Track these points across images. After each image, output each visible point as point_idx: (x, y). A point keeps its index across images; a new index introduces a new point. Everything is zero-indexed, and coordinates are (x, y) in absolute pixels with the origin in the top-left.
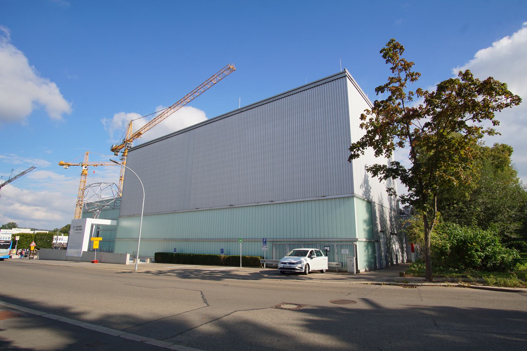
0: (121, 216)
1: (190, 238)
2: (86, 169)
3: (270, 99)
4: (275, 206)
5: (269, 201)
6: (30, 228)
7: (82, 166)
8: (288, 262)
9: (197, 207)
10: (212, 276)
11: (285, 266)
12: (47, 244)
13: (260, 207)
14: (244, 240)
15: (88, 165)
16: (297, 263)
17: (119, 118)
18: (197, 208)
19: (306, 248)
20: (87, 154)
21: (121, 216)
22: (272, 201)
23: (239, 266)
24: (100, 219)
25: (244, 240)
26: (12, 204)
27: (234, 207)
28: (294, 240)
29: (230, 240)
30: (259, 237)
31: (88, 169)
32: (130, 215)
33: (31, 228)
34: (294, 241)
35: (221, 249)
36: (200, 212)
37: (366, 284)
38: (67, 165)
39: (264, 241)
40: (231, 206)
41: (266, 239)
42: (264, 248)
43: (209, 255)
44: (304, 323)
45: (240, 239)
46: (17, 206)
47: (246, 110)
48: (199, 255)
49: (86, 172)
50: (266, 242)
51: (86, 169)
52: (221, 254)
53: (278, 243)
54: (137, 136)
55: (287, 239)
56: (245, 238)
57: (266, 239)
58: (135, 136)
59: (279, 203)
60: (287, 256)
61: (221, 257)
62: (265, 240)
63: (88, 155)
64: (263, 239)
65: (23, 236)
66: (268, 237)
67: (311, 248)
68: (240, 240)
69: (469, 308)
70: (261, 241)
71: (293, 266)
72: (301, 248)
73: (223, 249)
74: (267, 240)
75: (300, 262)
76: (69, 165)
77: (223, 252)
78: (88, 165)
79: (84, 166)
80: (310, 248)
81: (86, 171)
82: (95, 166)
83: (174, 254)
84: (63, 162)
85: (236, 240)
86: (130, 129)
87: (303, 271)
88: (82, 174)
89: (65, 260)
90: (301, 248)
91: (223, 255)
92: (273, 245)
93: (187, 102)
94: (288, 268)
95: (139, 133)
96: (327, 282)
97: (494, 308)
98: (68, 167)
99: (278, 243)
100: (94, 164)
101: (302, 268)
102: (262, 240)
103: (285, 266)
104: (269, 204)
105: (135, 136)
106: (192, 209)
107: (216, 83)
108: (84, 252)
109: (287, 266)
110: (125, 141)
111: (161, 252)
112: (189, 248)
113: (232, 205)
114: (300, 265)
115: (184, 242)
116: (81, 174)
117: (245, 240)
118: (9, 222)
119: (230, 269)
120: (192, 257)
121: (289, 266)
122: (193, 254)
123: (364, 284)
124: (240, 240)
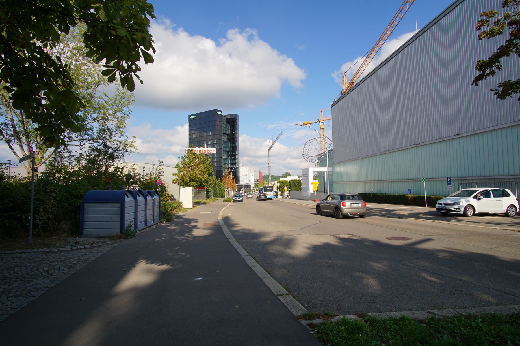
0: (334, 163)
1: (384, 179)
2: (323, 124)
3: (448, 8)
4: (461, 140)
5: (455, 135)
6: (297, 176)
7: (319, 122)
8: (443, 203)
9: (416, 142)
10: (390, 214)
11: (440, 207)
12: (298, 188)
13: (444, 143)
14: (428, 180)
15: (323, 121)
16: (454, 204)
17: (346, 67)
18: (387, 151)
19: (472, 188)
20: (321, 111)
21: (334, 163)
22: (458, 135)
23: (425, 206)
24: (320, 167)
25: (428, 180)
26: (286, 159)
27: (419, 146)
28: (515, 177)
29: (418, 180)
30: (443, 176)
31: (324, 124)
32: (339, 162)
33: (298, 175)
34: (485, 179)
35: (409, 189)
36: (390, 154)
37: (512, 230)
38: (308, 124)
39: (449, 180)
40: (417, 145)
41: (450, 177)
42: (449, 188)
43: (399, 196)
44: (237, 226)
45: (424, 179)
46: (289, 160)
47: (422, 34)
48: (390, 195)
49: (323, 127)
50: (450, 181)
51: (323, 124)
52: (410, 194)
53: (466, 182)
54: (350, 86)
55: (504, 175)
56: (419, 178)
57: (450, 177)
58: (349, 86)
59: (500, 128)
60: (450, 196)
61: (408, 197)
62: (449, 179)
63: (322, 112)
64: (448, 178)
65: (282, 182)
66: (452, 176)
67: (481, 187)
68: (424, 180)
69: (447, 248)
70: (445, 180)
71: (448, 207)
72: (473, 187)
73: (410, 189)
74: (451, 179)
75: (458, 204)
76: (310, 124)
77: (410, 192)
78: (323, 121)
79: (321, 122)
80: (480, 187)
81: (322, 126)
82: (329, 120)
83: (371, 195)
84: (306, 122)
85: (418, 180)
86: (344, 81)
87: (462, 213)
88: (320, 129)
89: (302, 199)
90: (473, 187)
91: (411, 196)
92: (459, 184)
93: (387, 36)
94: (442, 209)
95: (352, 82)
96: (468, 225)
97: (480, 252)
98: (310, 126)
99: (466, 182)
100: (328, 119)
101: (459, 209)
102: (447, 179)
103: (440, 206)
104: (425, 145)
105: (349, 86)
106: (383, 152)
107: (413, 2)
108: (311, 193)
109: (442, 207)
110: (342, 93)
111: (364, 192)
112: (471, 185)
113: (418, 144)
114: (456, 207)
115: (408, 182)
116: (320, 129)
117: (429, 180)
118: (286, 172)
119: (409, 207)
120: (385, 197)
121: (444, 207)
122: (386, 194)
123: (510, 230)
124: (424, 180)
